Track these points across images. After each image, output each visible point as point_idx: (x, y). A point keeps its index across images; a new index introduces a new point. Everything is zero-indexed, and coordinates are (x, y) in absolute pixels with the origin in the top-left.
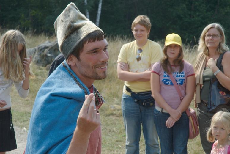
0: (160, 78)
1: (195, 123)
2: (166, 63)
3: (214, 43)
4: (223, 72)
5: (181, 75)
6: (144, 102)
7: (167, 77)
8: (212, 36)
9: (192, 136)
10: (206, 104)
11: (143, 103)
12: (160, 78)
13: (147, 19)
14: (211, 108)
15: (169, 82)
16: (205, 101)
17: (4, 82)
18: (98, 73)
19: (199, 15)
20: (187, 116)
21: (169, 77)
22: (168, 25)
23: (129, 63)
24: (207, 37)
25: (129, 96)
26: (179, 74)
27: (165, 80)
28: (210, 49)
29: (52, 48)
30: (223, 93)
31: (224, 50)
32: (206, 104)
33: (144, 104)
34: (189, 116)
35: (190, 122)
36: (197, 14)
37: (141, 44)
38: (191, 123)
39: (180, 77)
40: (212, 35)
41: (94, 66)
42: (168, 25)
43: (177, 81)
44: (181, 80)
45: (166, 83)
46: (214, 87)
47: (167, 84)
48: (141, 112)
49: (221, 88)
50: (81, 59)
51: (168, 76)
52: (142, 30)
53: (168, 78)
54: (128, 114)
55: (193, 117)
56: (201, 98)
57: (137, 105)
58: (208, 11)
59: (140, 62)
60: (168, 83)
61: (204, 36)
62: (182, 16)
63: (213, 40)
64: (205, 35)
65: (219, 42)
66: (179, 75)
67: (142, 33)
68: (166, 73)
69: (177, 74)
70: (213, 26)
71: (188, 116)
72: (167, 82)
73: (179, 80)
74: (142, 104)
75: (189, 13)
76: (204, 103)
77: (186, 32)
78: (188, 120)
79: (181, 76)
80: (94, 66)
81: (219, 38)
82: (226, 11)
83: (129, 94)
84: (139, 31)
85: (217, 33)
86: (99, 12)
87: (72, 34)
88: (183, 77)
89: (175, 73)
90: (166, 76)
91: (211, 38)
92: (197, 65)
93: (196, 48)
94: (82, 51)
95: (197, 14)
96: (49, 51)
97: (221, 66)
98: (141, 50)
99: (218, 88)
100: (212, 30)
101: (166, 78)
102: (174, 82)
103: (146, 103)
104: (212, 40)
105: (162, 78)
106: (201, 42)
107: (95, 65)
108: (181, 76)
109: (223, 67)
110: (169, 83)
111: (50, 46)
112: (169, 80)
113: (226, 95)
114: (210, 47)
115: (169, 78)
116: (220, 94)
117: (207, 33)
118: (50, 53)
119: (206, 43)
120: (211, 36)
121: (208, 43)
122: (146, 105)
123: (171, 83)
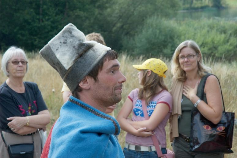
4: (207, 103)
5: (153, 106)
7: (139, 106)
10: (186, 139)
15: (140, 112)
16: (185, 135)
18: (117, 95)
19: (48, 20)
22: (15, 31)
23: (30, 86)
27: (135, 110)
30: (207, 128)
31: (204, 76)
32: (186, 139)
36: (47, 18)
39: (151, 107)
40: (186, 56)
41: (114, 87)
42: (15, 31)
45: (137, 113)
46: (197, 118)
47: (136, 115)
49: (205, 121)
50: (99, 80)
51: (140, 106)
56: (179, 131)
58: (57, 14)
60: (139, 113)
62: (30, 21)
64: (179, 58)
70: (185, 45)
72: (138, 113)
75: (38, 17)
76: (184, 138)
77: (35, 37)
79: (152, 106)
80: (114, 87)
81: (196, 57)
82: (76, 14)
85: (192, 52)
87: (88, 52)
88: (154, 107)
94: (101, 70)
95: (47, 18)
97: (204, 94)
99: (201, 121)
100: (185, 50)
107: (115, 86)
108: (152, 106)
109: (206, 95)
110: (140, 113)
112: (139, 110)
113: (211, 129)
115: (141, 108)
116: (205, 129)
117: (180, 55)
119: (182, 66)
120: (185, 57)
121: (184, 65)
123: (141, 114)
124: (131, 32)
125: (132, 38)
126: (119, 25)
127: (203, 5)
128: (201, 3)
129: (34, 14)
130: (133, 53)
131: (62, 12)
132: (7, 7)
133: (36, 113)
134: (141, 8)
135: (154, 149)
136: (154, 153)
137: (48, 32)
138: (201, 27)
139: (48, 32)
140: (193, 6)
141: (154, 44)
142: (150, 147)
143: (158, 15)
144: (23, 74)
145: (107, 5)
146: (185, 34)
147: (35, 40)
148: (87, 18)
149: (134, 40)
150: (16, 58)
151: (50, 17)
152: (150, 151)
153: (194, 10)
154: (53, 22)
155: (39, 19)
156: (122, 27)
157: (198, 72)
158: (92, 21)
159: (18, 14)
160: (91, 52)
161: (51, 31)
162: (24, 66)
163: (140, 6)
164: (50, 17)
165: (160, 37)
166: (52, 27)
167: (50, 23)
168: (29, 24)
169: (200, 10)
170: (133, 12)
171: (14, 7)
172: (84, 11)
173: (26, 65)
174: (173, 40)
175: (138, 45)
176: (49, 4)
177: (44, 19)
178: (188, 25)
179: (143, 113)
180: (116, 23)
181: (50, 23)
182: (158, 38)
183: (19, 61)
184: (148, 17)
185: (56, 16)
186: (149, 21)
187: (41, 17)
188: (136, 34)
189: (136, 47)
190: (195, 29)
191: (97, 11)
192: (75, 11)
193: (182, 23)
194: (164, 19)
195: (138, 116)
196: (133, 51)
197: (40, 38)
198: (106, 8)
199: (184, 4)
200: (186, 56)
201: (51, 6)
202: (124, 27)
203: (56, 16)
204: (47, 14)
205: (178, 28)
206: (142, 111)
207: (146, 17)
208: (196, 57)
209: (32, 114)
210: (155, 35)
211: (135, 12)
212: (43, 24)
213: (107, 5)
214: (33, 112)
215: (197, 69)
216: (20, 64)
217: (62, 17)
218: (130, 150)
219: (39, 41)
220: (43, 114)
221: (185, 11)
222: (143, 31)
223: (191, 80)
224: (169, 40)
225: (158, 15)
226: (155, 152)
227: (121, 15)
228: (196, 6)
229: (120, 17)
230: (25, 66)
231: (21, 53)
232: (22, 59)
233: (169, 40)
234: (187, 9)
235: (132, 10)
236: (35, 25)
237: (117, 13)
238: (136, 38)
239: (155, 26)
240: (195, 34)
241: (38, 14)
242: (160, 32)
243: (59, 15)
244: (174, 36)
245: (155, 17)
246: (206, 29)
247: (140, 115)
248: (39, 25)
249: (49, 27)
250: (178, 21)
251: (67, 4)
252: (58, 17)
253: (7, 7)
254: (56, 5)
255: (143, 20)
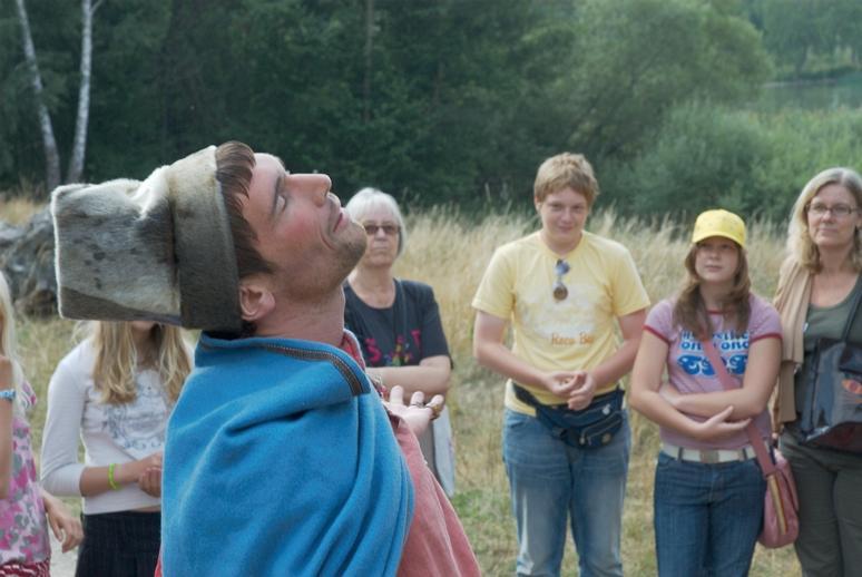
0: (669, 353)
1: (786, 499)
2: (692, 306)
3: (835, 231)
5: (738, 344)
6: (583, 435)
8: (831, 210)
9: (775, 538)
11: (578, 437)
12: (669, 353)
13: (586, 168)
14: (812, 431)
15: (700, 363)
17: (147, 419)
19: (389, 111)
20: (761, 472)
21: (699, 348)
22: (296, 143)
24: (815, 212)
25: (531, 417)
26: (732, 338)
27: (685, 360)
28: (822, 252)
29: (26, 245)
33: (582, 441)
34: (767, 476)
35: (768, 493)
36: (385, 106)
37: (564, 243)
38: (773, 496)
40: (829, 206)
43: (725, 362)
44: (737, 359)
47: (690, 373)
48: (571, 467)
52: (576, 208)
53: (695, 352)
54: (523, 477)
55: (781, 478)
57: (561, 444)
58: (412, 96)
59: (565, 305)
61: (806, 210)
62: (338, 115)
63: (835, 221)
65: (852, 231)
66: (730, 342)
67: (577, 216)
68: (691, 337)
69: (726, 338)
70: (834, 179)
71: (765, 473)
72: (695, 366)
73: (732, 360)
74: (578, 440)
75: (360, 105)
77: (351, 163)
78: (764, 485)
81: (854, 215)
82: (467, 95)
83: (531, 411)
84: (567, 209)
86: (84, 114)
89: (719, 336)
90: (728, 346)
91: (826, 215)
92: (782, 298)
93: (784, 245)
95: (385, 106)
96: (16, 254)
98: (564, 268)
101: (690, 352)
102: (716, 365)
103: (589, 438)
104: (829, 222)
105: (678, 354)
106: (795, 227)
111: (16, 239)
112: (699, 359)
114: (825, 246)
115: (701, 351)
118: (21, 262)
120: (826, 209)
122: (590, 443)
124: (624, 148)
125: (626, 165)
126: (587, 126)
127: (837, 65)
128: (830, 61)
129: (350, 95)
130: (631, 207)
131: (426, 89)
132: (275, 76)
133: (415, 362)
134: (654, 78)
135: (751, 453)
136: (753, 463)
137: (387, 149)
138: (830, 133)
139: (387, 149)
140: (805, 69)
141: (690, 182)
142: (744, 451)
143: (703, 98)
144: (388, 259)
145: (555, 69)
146: (784, 153)
147: (351, 171)
148: (496, 105)
149: (632, 169)
150: (371, 218)
151: (393, 105)
152: (742, 459)
153: (808, 82)
154: (402, 120)
155: (362, 111)
156: (597, 131)
157: (850, 256)
158: (510, 115)
159: (305, 97)
160: (187, 232)
161: (394, 144)
162: (390, 238)
163: (650, 71)
164: (393, 105)
165: (710, 161)
166: (397, 133)
167: (392, 122)
168: (335, 122)
169: (826, 81)
170: (630, 89)
171: (294, 78)
172: (489, 87)
173: (397, 236)
174: (749, 170)
175: (647, 184)
176: (393, 68)
177: (376, 111)
178: (793, 126)
179: (709, 366)
180: (580, 121)
181: (392, 122)
182: (704, 164)
183: (379, 224)
184: (675, 103)
185: (409, 101)
186: (677, 114)
187: (368, 104)
188: (639, 152)
189: (639, 191)
190: (814, 138)
191: (525, 86)
192: (463, 87)
193: (775, 119)
194: (719, 109)
195: (697, 375)
196: (631, 202)
197: (364, 164)
198: (553, 77)
199: (778, 64)
200: (829, 206)
201: (395, 73)
202: (604, 131)
203: (409, 101)
204: (385, 96)
205: (761, 134)
206: (705, 361)
207: (669, 104)
208: (854, 215)
209: (403, 364)
210: (696, 157)
211: (635, 88)
212: (372, 125)
213: (555, 69)
214: (406, 359)
215: (851, 245)
216: (381, 233)
217: (427, 104)
218: (685, 463)
219: (361, 174)
220: (430, 365)
221: (782, 84)
222: (661, 143)
223: (832, 271)
224: (736, 169)
225: (703, 98)
226: (756, 460)
227: (595, 96)
228: (815, 69)
229: (593, 103)
230: (393, 240)
231: (383, 206)
232: (387, 219)
233: (736, 169)
234: (789, 79)
235: (627, 83)
236: (352, 127)
237: (584, 92)
238: (641, 164)
239: (694, 128)
240: (814, 151)
241: (359, 95)
242: (710, 145)
243: (419, 98)
244: (751, 158)
245: (696, 104)
246: (848, 137)
247: (703, 371)
248: (363, 129)
249: (391, 134)
250: (764, 115)
251: (442, 66)
252: (416, 103)
253: (275, 76)
254: (411, 70)
255: (660, 111)
